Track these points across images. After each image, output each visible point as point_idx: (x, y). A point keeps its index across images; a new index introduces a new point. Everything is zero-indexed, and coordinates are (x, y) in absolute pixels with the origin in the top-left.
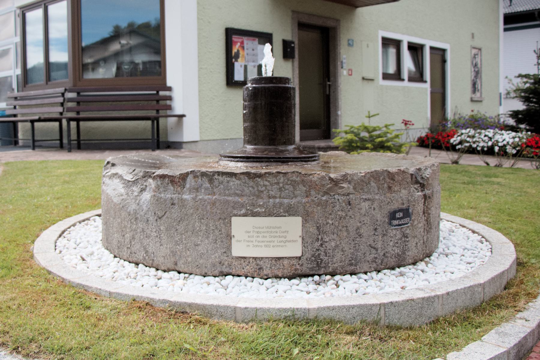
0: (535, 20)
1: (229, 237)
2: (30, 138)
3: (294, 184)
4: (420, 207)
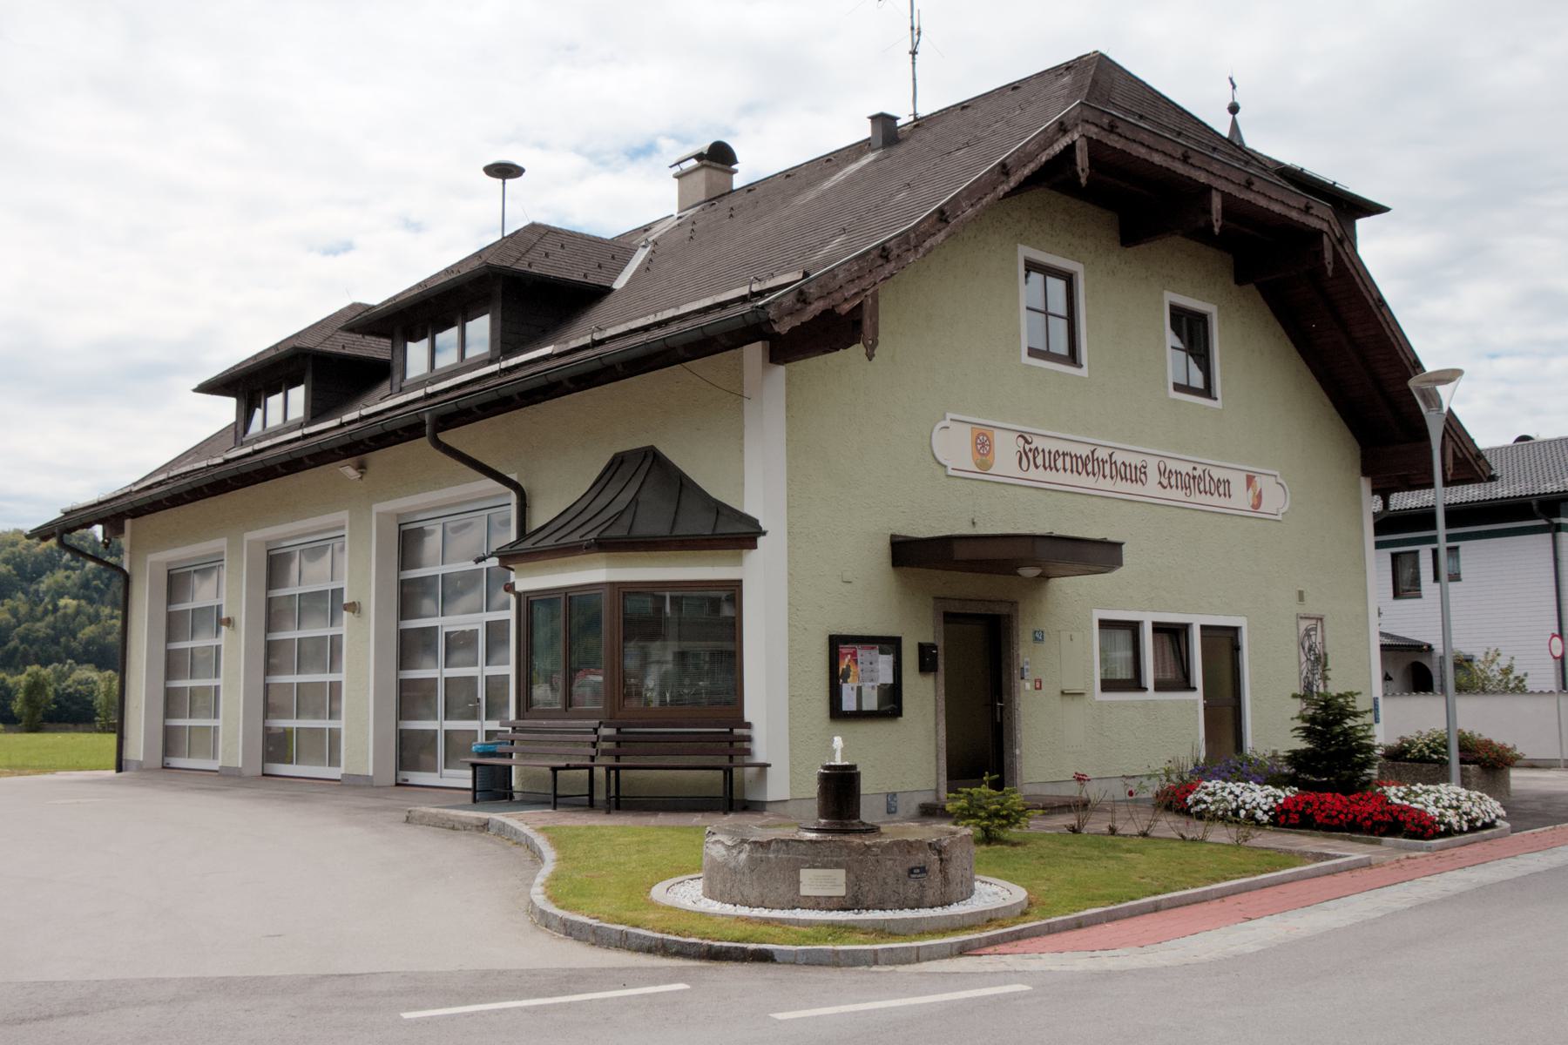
0: (1533, 517)
1: (798, 882)
2: (551, 791)
3: (841, 848)
4: (937, 866)
